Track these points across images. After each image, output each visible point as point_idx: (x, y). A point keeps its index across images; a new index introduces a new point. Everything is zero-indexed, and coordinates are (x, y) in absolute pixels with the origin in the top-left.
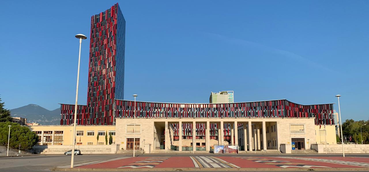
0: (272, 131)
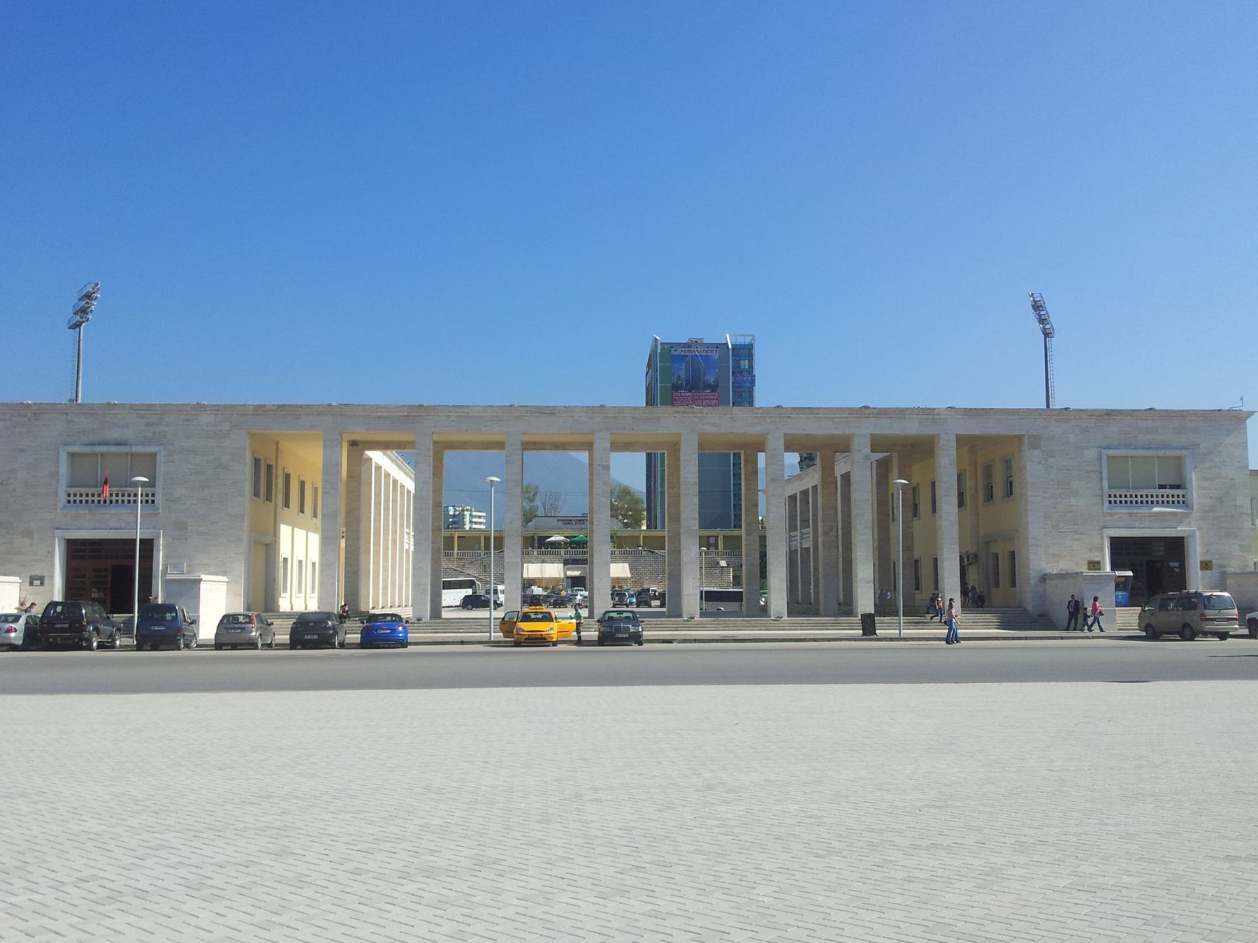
0: (990, 496)
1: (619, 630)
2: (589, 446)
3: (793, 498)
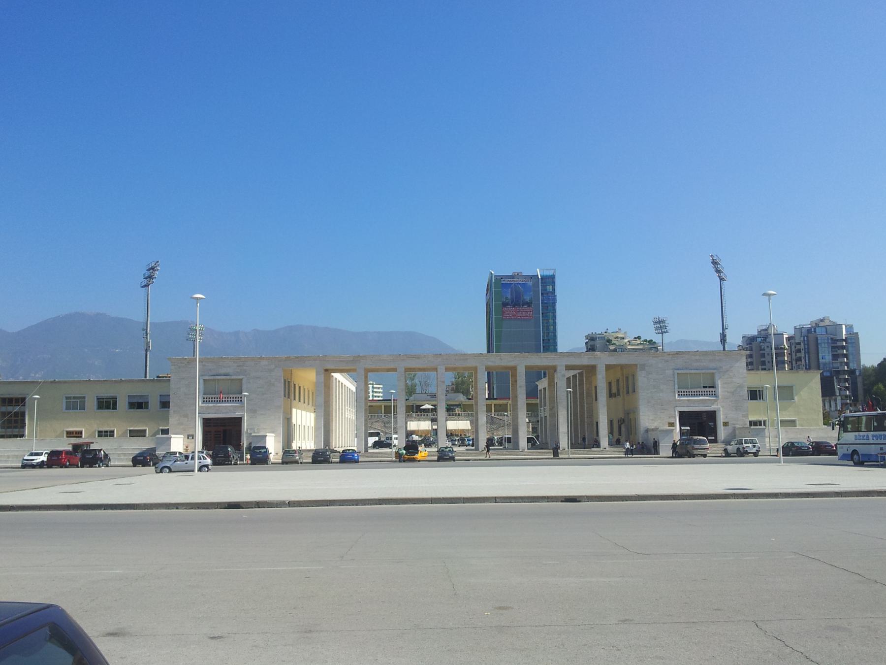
0: (628, 392)
1: (445, 455)
2: (436, 369)
3: (568, 379)
